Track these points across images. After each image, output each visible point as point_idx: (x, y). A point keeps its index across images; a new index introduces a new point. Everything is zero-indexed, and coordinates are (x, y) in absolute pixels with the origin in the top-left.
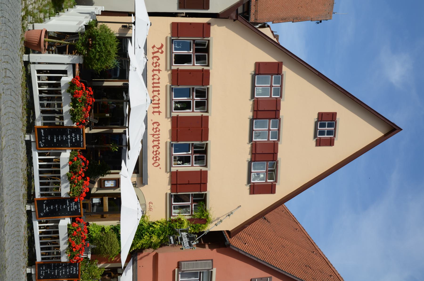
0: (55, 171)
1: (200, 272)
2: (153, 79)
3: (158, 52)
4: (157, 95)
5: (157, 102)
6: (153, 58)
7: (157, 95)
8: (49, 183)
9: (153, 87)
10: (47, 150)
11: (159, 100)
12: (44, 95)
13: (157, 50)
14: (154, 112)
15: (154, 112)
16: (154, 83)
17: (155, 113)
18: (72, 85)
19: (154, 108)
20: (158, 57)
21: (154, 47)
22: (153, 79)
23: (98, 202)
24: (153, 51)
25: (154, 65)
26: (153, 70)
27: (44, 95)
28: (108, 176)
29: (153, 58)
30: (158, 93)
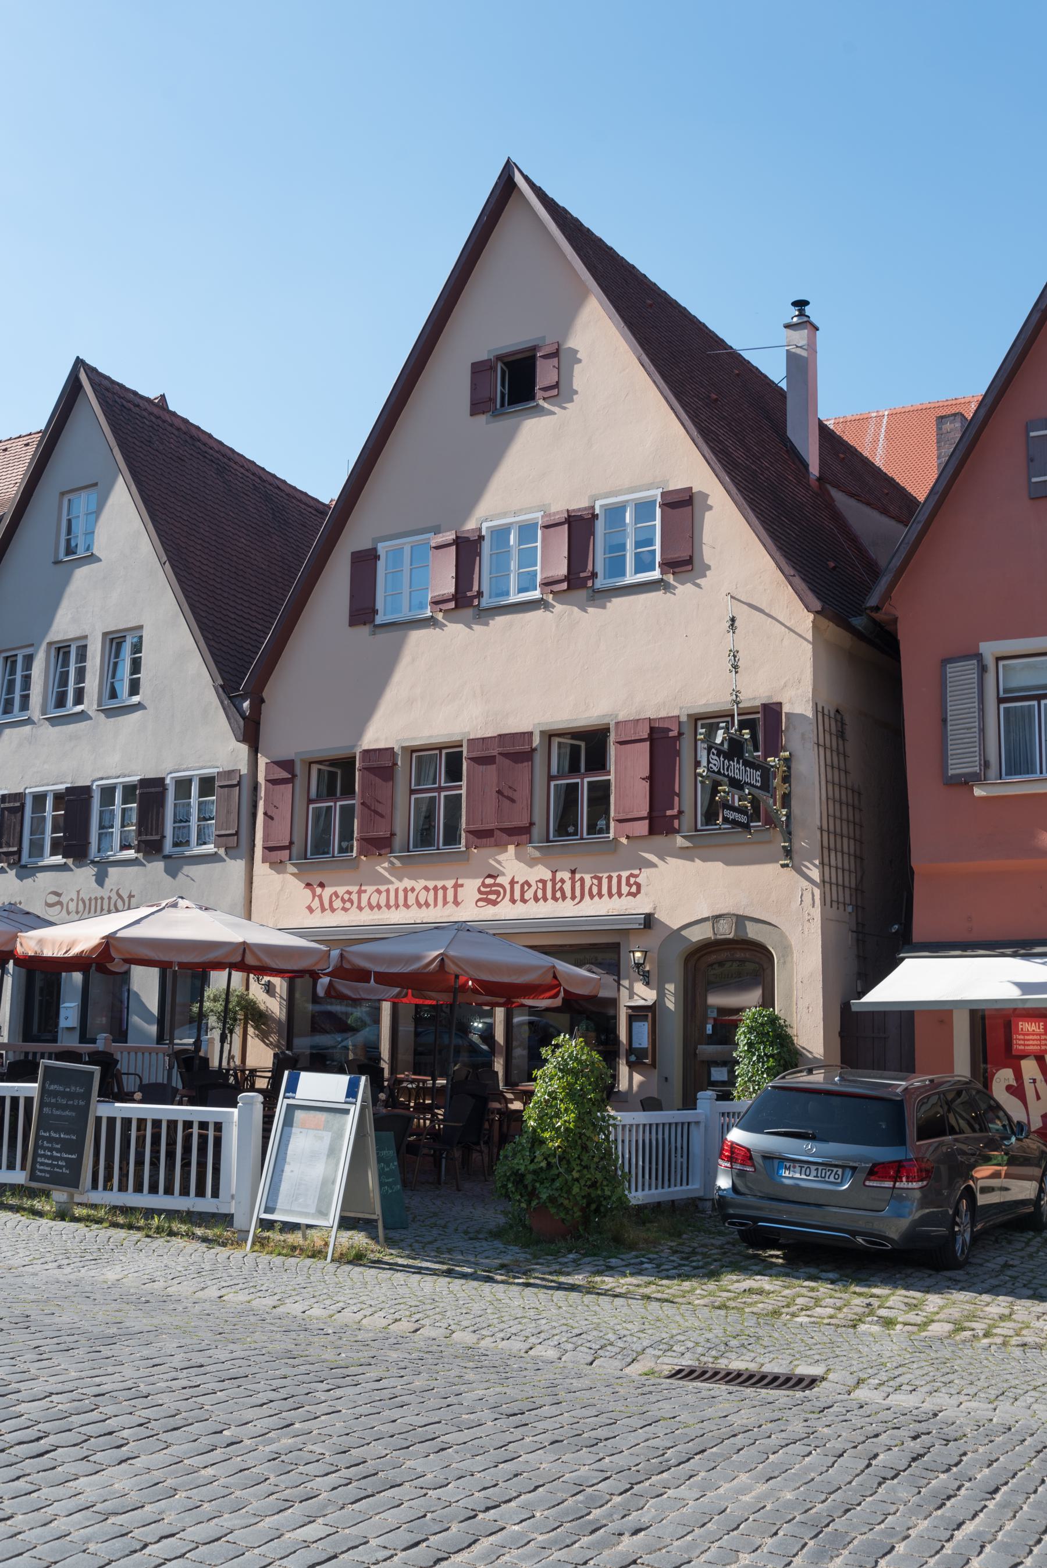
0: (138, 1129)
1: (397, 906)
2: (379, 907)
3: (320, 897)
4: (415, 893)
5: (432, 893)
6: (333, 910)
7: (415, 893)
8: (200, 1136)
9: (397, 906)
10: (637, 1167)
11: (426, 889)
12: (195, 1131)
13: (317, 898)
14: (456, 903)
15: (456, 903)
16: (388, 906)
17: (459, 900)
18: (842, 1079)
19: (445, 903)
20: (331, 897)
21: (310, 909)
22: (379, 907)
23: (265, 1087)
24: (319, 909)
25: (348, 905)
26: (360, 908)
27: (195, 1131)
28: (623, 1037)
29: (333, 910)
30: (409, 893)
